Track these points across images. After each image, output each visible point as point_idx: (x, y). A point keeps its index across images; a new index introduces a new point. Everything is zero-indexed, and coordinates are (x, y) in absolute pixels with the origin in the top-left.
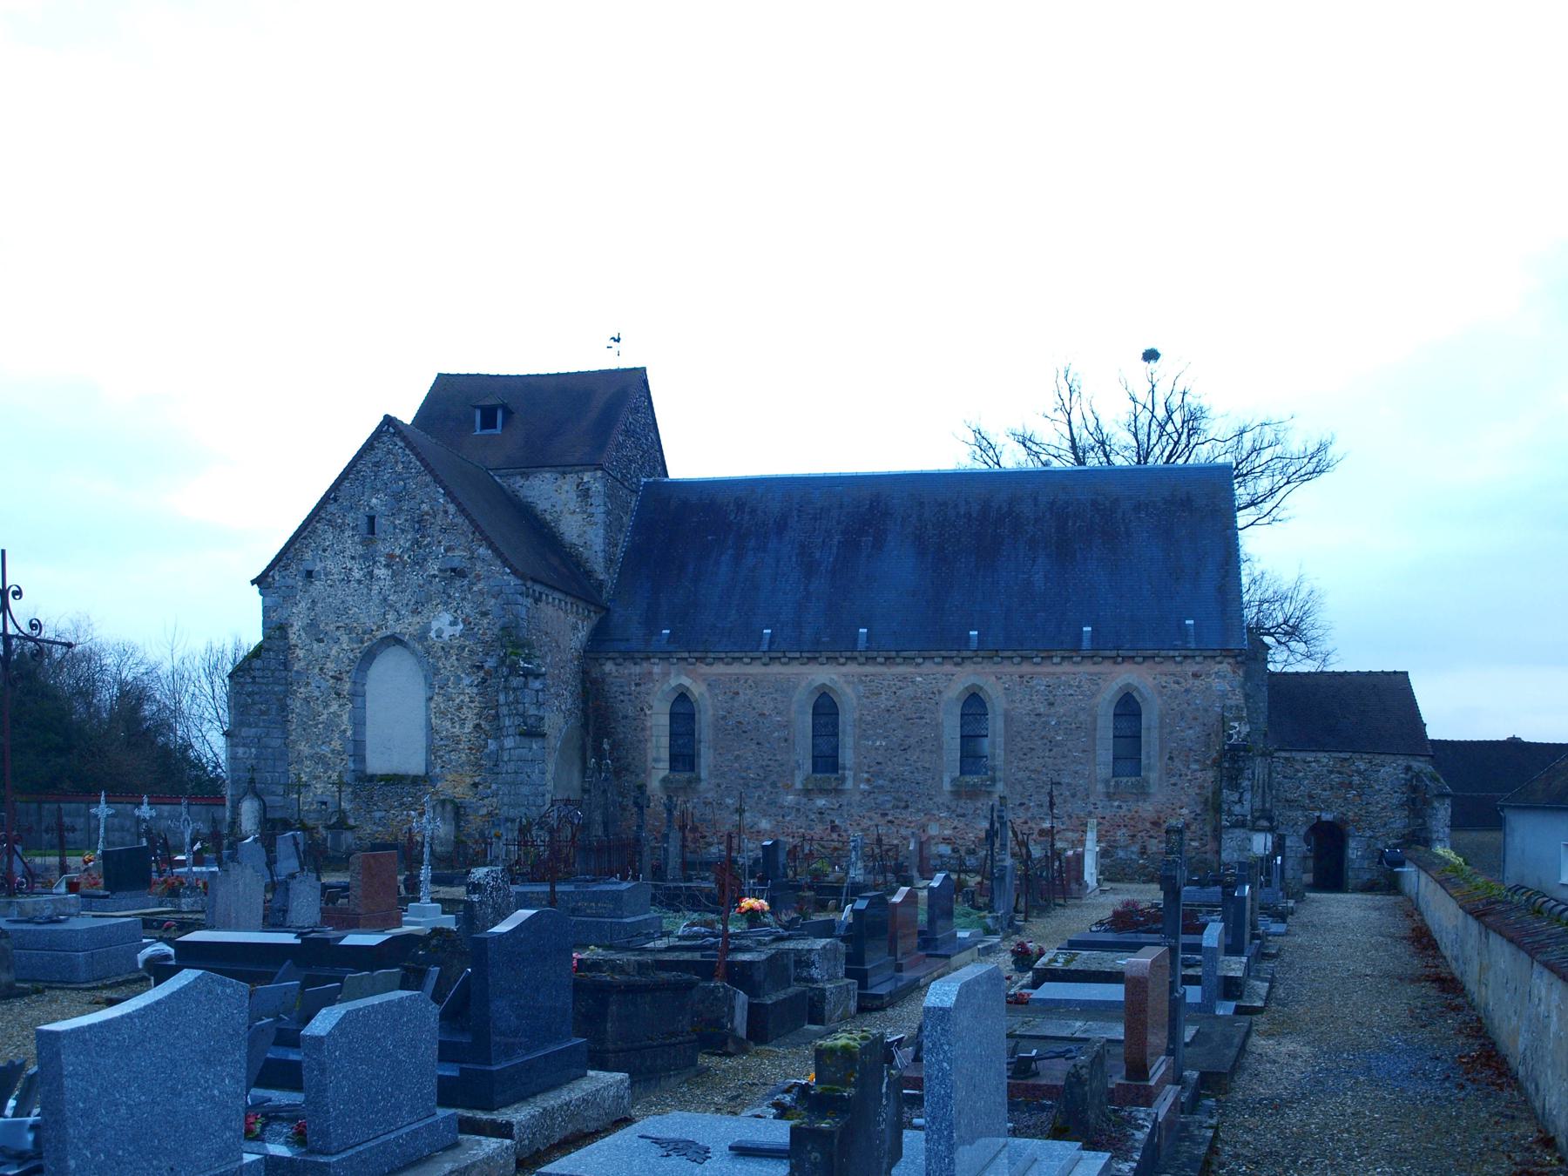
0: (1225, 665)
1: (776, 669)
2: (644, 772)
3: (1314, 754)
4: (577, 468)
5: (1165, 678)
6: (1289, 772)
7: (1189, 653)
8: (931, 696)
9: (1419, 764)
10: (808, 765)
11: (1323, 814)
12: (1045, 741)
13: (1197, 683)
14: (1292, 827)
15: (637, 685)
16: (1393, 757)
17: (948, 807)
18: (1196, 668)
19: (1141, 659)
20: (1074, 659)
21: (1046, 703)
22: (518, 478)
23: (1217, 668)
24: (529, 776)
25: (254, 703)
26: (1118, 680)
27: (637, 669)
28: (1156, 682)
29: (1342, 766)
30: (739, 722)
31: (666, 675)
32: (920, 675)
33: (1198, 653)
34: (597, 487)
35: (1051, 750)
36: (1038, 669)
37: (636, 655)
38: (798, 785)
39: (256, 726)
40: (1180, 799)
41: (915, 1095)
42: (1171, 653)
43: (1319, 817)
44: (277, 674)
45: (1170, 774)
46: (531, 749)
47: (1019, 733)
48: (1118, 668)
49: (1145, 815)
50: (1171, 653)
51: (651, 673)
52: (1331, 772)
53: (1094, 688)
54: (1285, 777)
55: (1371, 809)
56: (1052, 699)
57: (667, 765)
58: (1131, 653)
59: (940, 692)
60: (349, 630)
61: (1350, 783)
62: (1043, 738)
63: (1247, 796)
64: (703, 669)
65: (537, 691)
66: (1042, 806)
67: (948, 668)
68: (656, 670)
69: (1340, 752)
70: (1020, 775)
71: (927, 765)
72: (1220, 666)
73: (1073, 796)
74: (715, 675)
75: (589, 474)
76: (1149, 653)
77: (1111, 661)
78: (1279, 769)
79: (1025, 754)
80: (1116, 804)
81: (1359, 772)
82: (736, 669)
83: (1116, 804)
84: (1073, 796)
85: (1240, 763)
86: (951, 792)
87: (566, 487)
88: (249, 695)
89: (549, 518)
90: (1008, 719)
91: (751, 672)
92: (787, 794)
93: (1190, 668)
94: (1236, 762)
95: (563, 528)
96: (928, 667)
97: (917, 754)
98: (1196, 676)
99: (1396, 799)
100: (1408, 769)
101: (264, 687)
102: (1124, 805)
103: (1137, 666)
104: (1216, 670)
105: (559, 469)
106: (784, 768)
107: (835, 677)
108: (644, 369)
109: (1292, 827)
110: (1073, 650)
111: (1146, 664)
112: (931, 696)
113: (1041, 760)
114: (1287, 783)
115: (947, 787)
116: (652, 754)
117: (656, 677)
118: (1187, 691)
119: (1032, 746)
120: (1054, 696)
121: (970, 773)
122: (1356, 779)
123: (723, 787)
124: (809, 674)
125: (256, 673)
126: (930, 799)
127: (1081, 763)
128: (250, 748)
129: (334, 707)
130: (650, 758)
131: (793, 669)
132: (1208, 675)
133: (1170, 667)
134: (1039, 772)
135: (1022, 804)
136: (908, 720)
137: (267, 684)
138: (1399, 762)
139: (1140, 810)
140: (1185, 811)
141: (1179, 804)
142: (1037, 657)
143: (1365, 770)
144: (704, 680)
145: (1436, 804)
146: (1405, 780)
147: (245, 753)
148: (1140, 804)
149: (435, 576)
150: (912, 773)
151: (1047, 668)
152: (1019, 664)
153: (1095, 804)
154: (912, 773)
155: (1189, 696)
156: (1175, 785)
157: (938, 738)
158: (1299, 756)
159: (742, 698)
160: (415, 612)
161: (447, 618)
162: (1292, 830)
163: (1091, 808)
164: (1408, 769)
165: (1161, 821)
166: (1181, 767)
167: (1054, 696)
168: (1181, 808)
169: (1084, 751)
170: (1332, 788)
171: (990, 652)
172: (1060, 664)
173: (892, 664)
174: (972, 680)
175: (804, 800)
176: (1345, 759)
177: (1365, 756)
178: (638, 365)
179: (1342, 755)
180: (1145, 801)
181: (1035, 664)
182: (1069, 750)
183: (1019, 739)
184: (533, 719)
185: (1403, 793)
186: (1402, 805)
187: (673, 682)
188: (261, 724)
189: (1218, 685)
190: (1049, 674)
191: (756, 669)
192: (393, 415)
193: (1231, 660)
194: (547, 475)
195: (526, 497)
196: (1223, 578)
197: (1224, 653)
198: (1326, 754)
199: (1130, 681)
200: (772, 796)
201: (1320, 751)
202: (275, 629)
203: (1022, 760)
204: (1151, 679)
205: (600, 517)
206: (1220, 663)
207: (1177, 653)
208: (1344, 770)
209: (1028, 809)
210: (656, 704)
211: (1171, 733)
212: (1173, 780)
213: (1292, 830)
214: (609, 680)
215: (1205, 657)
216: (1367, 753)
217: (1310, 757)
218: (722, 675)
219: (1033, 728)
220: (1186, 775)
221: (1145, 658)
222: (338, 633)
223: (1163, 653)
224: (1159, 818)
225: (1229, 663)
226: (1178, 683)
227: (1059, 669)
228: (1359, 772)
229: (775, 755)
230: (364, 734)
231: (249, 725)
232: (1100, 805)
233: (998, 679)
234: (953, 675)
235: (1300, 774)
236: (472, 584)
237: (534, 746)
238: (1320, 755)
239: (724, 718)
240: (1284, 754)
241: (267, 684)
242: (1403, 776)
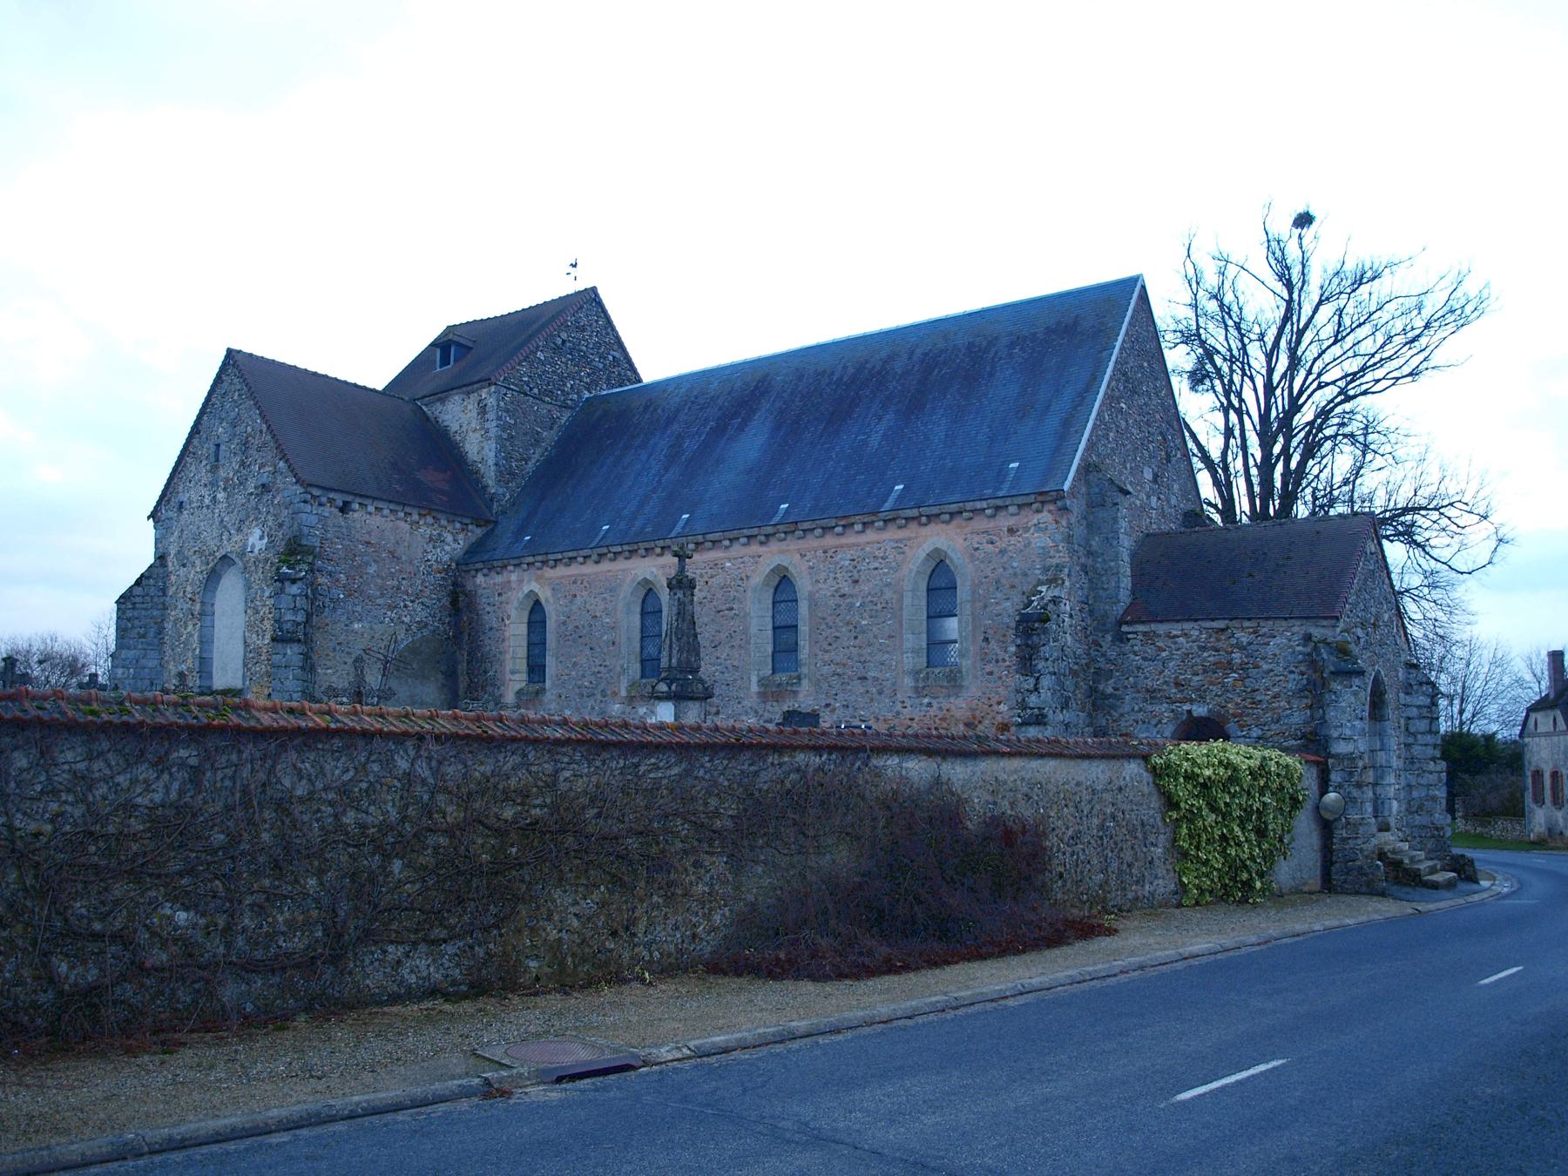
0: (1045, 513)
1: (606, 566)
2: (503, 685)
3: (1179, 626)
4: (475, 386)
5: (977, 538)
6: (1150, 651)
7: (999, 502)
8: (740, 583)
9: (1322, 630)
10: (636, 668)
11: (1194, 707)
12: (851, 627)
13: (1013, 540)
14: (1156, 726)
15: (500, 595)
16: (1284, 623)
17: (756, 712)
18: (1012, 521)
19: (947, 517)
20: (876, 524)
21: (850, 581)
22: (438, 404)
23: (1035, 519)
24: (282, 683)
25: (133, 627)
26: (925, 546)
27: (498, 579)
28: (967, 543)
29: (1218, 640)
30: (577, 627)
31: (521, 581)
32: (730, 560)
33: (1008, 501)
34: (491, 401)
35: (856, 638)
36: (843, 540)
37: (495, 563)
38: (623, 693)
39: (135, 648)
40: (997, 693)
41: (1275, 1068)
42: (979, 505)
43: (1189, 712)
44: (155, 599)
45: (985, 659)
46: (285, 654)
47: (824, 619)
48: (925, 531)
49: (958, 714)
50: (979, 505)
51: (509, 582)
52: (1203, 649)
53: (900, 558)
54: (1145, 659)
55: (1259, 698)
56: (856, 576)
57: (524, 676)
58: (935, 510)
59: (748, 577)
60: (200, 552)
61: (1229, 662)
62: (848, 624)
63: (1046, 682)
64: (549, 573)
65: (294, 596)
66: (848, 707)
67: (755, 548)
68: (514, 577)
69: (1213, 620)
70: (825, 670)
71: (735, 664)
72: (1040, 516)
73: (880, 693)
74: (557, 578)
75: (485, 390)
76: (954, 507)
77: (916, 523)
78: (1136, 648)
79: (830, 644)
80: (926, 701)
81: (1242, 648)
82: (575, 570)
83: (926, 701)
84: (880, 693)
85: (1035, 638)
86: (759, 693)
87: (470, 407)
88: (129, 620)
89: (458, 438)
90: (814, 604)
91: (586, 572)
92: (614, 703)
93: (1004, 521)
94: (1029, 636)
95: (468, 447)
96: (736, 550)
97: (727, 650)
98: (1011, 531)
99: (1293, 682)
100: (1308, 638)
101: (143, 612)
102: (934, 703)
103: (944, 526)
104: (1035, 521)
105: (464, 389)
106: (611, 674)
107: (654, 569)
108: (594, 289)
109: (1156, 726)
110: (872, 516)
111: (955, 522)
112: (740, 583)
113: (846, 651)
114: (1149, 667)
115: (754, 688)
116: (509, 666)
117: (514, 585)
118: (1002, 552)
119: (837, 634)
120: (859, 571)
121: (784, 670)
122: (1237, 657)
123: (563, 697)
124: (634, 569)
125: (138, 600)
126: (739, 703)
127: (888, 652)
128: (128, 669)
129: (190, 627)
130: (507, 669)
131: (621, 564)
132: (1027, 529)
133: (980, 523)
134: (844, 665)
135: (827, 705)
136: (719, 612)
137: (146, 609)
138: (1295, 629)
139: (953, 708)
140: (1003, 708)
141: (997, 698)
142: (837, 526)
143: (1250, 644)
144: (549, 584)
145: (1335, 686)
146: (1304, 654)
147: (123, 673)
148: (952, 700)
149: (251, 494)
150: (723, 673)
151: (850, 539)
152: (822, 536)
153: (903, 702)
154: (723, 673)
155: (1005, 559)
156: (991, 673)
157: (745, 632)
158: (1162, 628)
159: (579, 600)
160: (239, 530)
161: (257, 532)
162: (1155, 730)
163: (899, 707)
164: (1308, 638)
165: (976, 722)
166: (998, 651)
167: (859, 571)
168: (999, 703)
169: (890, 637)
170: (1205, 671)
171: (792, 528)
172: (863, 531)
173: (703, 550)
174: (777, 560)
175: (628, 709)
176: (1223, 630)
177: (1247, 624)
178: (589, 286)
179: (1215, 624)
180: (957, 697)
181: (837, 535)
182: (875, 637)
183: (823, 627)
184: (289, 624)
185: (1302, 674)
186: (1301, 691)
187: (526, 590)
188: (140, 647)
189: (1039, 540)
190: (854, 545)
191: (590, 569)
192: (236, 347)
193: (1052, 507)
194: (456, 398)
195: (443, 421)
196: (1075, 408)
197: (1040, 498)
198: (1196, 625)
199: (939, 546)
200: (602, 705)
201: (1188, 620)
202: (161, 558)
203: (827, 652)
204: (962, 541)
205: (493, 432)
206: (1038, 511)
207: (984, 504)
208: (1220, 645)
209: (833, 711)
210: (513, 613)
211: (985, 607)
212: (988, 668)
213: (1155, 730)
214: (480, 591)
215: (1020, 506)
216: (1249, 619)
217: (1176, 629)
218: (563, 577)
219: (837, 612)
220: (1004, 660)
221: (952, 515)
222: (194, 557)
223: (969, 506)
224: (974, 718)
225: (1050, 511)
226: (992, 543)
227: (862, 539)
228: (1242, 648)
229: (605, 661)
230: (212, 652)
231: (129, 648)
232: (908, 703)
233: (803, 556)
234: (760, 556)
235: (1164, 654)
236: (274, 497)
237: (289, 651)
238: (1187, 626)
239: (564, 623)
240: (1141, 628)
241: (146, 609)
242: (1300, 648)
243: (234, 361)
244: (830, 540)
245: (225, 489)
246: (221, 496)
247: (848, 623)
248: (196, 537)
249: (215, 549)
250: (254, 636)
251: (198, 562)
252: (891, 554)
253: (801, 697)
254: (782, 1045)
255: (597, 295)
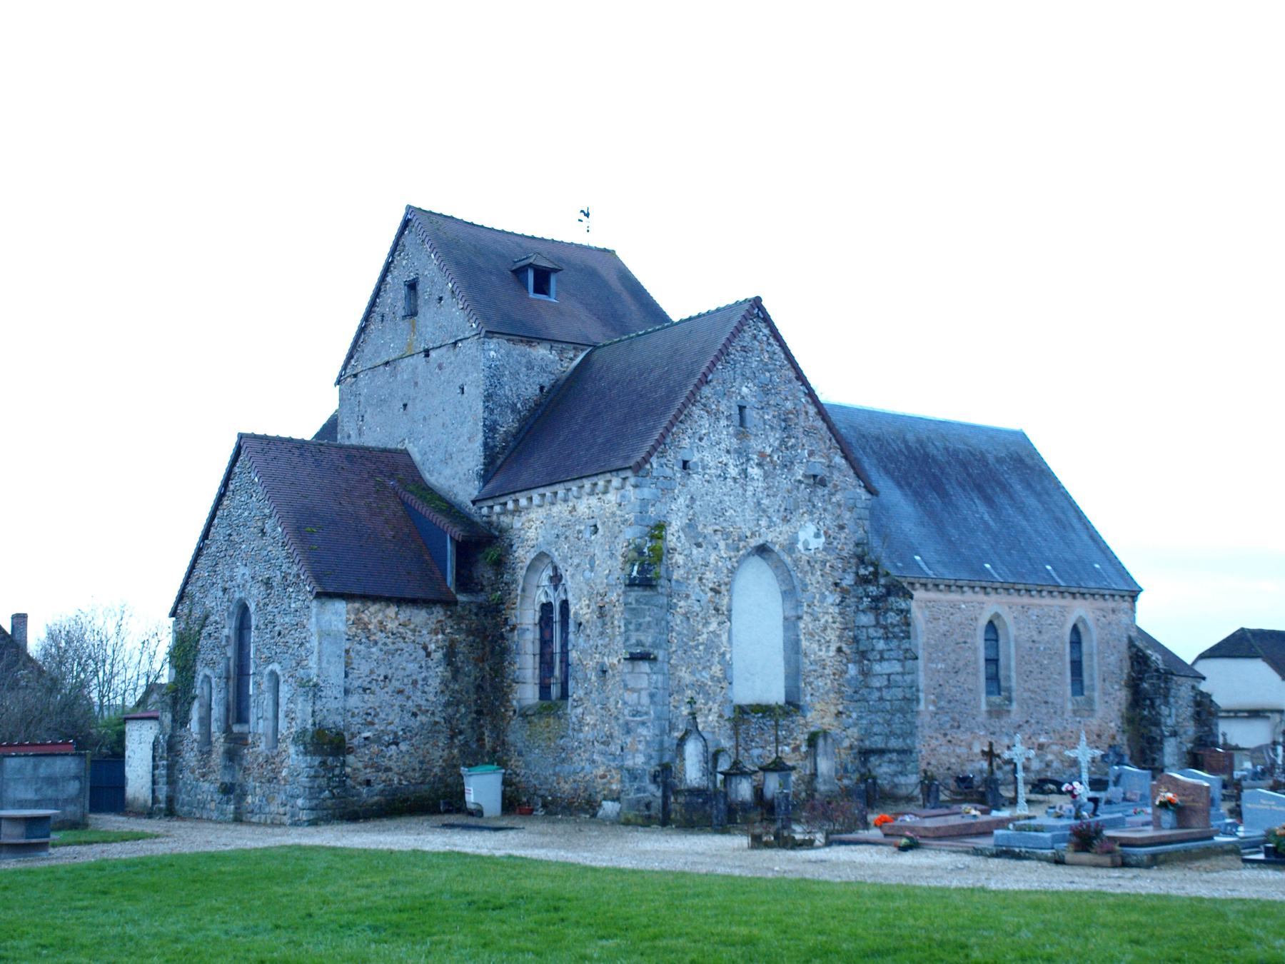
32: (964, 603)
67: (981, 597)
83: (1078, 719)
160: (786, 520)
161: (811, 528)
222: (716, 538)
243: (412, 221)
244: (1026, 600)
245: (760, 465)
246: (755, 472)
247: (1037, 662)
248: (720, 513)
249: (749, 534)
250: (815, 646)
251: (722, 545)
252: (1058, 616)
253: (1012, 715)
254: (732, 949)
255: (761, 308)
